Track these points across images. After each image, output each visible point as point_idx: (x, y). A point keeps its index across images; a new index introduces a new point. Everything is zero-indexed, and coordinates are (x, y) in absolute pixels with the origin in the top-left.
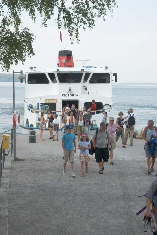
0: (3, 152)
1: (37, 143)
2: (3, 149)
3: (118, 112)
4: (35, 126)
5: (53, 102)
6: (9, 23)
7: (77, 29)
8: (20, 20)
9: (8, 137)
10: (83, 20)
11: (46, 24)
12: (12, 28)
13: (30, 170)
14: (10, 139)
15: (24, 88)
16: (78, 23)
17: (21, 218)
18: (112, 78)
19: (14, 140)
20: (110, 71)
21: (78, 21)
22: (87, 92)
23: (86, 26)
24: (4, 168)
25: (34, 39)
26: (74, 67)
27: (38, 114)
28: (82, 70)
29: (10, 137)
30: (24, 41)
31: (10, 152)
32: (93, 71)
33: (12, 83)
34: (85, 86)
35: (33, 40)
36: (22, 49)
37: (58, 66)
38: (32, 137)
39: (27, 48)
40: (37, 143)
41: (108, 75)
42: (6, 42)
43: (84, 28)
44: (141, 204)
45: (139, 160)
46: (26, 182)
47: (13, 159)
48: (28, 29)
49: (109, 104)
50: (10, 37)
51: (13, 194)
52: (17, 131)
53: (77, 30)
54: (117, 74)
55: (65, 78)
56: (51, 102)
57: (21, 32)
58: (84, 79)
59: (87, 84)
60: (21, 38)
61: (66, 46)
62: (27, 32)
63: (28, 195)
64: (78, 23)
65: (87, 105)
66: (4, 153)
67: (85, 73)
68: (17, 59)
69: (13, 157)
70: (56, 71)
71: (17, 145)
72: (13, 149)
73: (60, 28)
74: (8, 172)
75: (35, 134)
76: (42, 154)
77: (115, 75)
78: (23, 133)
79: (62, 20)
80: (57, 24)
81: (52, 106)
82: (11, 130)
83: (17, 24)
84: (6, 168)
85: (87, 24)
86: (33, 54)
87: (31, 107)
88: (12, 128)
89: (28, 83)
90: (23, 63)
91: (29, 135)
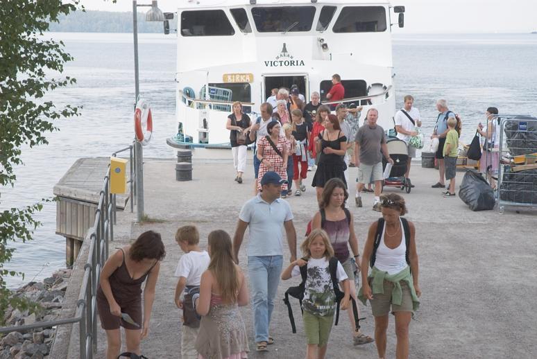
0: (111, 202)
1: (195, 180)
2: (111, 195)
4: (196, 141)
5: (243, 80)
14: (128, 170)
15: (175, 47)
18: (392, 17)
19: (138, 172)
22: (325, 54)
24: (114, 239)
27: (203, 110)
31: (129, 201)
33: (132, 35)
34: (323, 40)
38: (183, 166)
40: (195, 180)
41: (380, 10)
44: (448, 327)
45: (445, 221)
46: (166, 274)
47: (136, 220)
49: (382, 85)
54: (403, 7)
56: (238, 81)
58: (320, 19)
59: (329, 34)
63: (170, 303)
66: (114, 206)
69: (136, 215)
72: (135, 194)
75: (190, 159)
76: (208, 207)
77: (400, 10)
78: (160, 153)
81: (240, 92)
82: (131, 148)
87: (189, 93)
89: (183, 34)
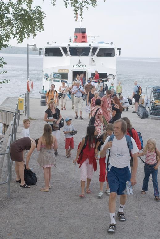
3: (3, 68)
5: (65, 72)
13: (41, 128)
14: (24, 102)
15: (42, 60)
16: (82, 2)
17: (32, 166)
18: (117, 52)
20: (115, 46)
22: (93, 63)
23: (89, 6)
25: (44, 17)
26: (87, 42)
28: (90, 45)
29: (25, 100)
30: (36, 18)
31: (25, 112)
33: (27, 55)
35: (43, 17)
36: (34, 25)
38: (43, 101)
39: (38, 24)
41: (112, 49)
42: (21, 18)
43: (87, 7)
48: (41, 8)
50: (24, 14)
54: (121, 48)
55: (75, 51)
56: (63, 72)
58: (92, 51)
59: (95, 57)
60: (34, 15)
62: (39, 10)
64: (82, 2)
67: (99, 48)
70: (68, 45)
71: (30, 107)
73: (67, 7)
77: (119, 49)
81: (64, 76)
82: (26, 94)
83: (29, 3)
85: (90, 4)
87: (47, 76)
88: (26, 93)
89: (45, 55)
90: (34, 38)
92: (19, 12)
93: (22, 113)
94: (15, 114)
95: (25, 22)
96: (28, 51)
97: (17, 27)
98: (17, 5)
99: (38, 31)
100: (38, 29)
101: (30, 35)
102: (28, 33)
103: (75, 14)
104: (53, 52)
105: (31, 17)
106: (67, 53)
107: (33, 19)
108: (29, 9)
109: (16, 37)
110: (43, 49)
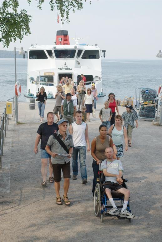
6: (8, 5)
7: (68, 11)
8: (18, 3)
9: (11, 104)
10: (73, 3)
11: (40, 7)
12: (10, 10)
14: (13, 106)
16: (68, 5)
17: (21, 171)
18: (101, 54)
21: (68, 4)
23: (75, 9)
25: (30, 20)
28: (76, 47)
30: (22, 22)
31: (13, 116)
32: (85, 48)
33: (14, 59)
37: (55, 44)
39: (24, 27)
42: (6, 22)
43: (73, 10)
47: (15, 123)
48: (26, 11)
49: (98, 77)
50: (10, 18)
51: (14, 151)
52: (19, 99)
53: (68, 12)
55: (60, 54)
56: (49, 75)
57: (20, 13)
61: (62, 28)
62: (25, 13)
64: (68, 5)
65: (80, 78)
68: (16, 37)
69: (16, 121)
70: (53, 48)
73: (53, 10)
74: (12, 134)
77: (104, 51)
79: (55, 3)
80: (50, 6)
81: (50, 79)
82: (14, 98)
84: (9, 130)
86: (30, 33)
87: (32, 79)
89: (30, 58)
91: (30, 103)
92: (5, 16)
93: (11, 118)
94: (2, 119)
95: (11, 26)
96: (15, 55)
97: (3, 31)
98: (2, 9)
99: (25, 35)
100: (25, 33)
101: (17, 39)
102: (14, 37)
103: (61, 17)
104: (38, 55)
105: (17, 20)
106: (51, 56)
107: (19, 22)
108: (14, 13)
109: (2, 40)
110: (27, 52)
